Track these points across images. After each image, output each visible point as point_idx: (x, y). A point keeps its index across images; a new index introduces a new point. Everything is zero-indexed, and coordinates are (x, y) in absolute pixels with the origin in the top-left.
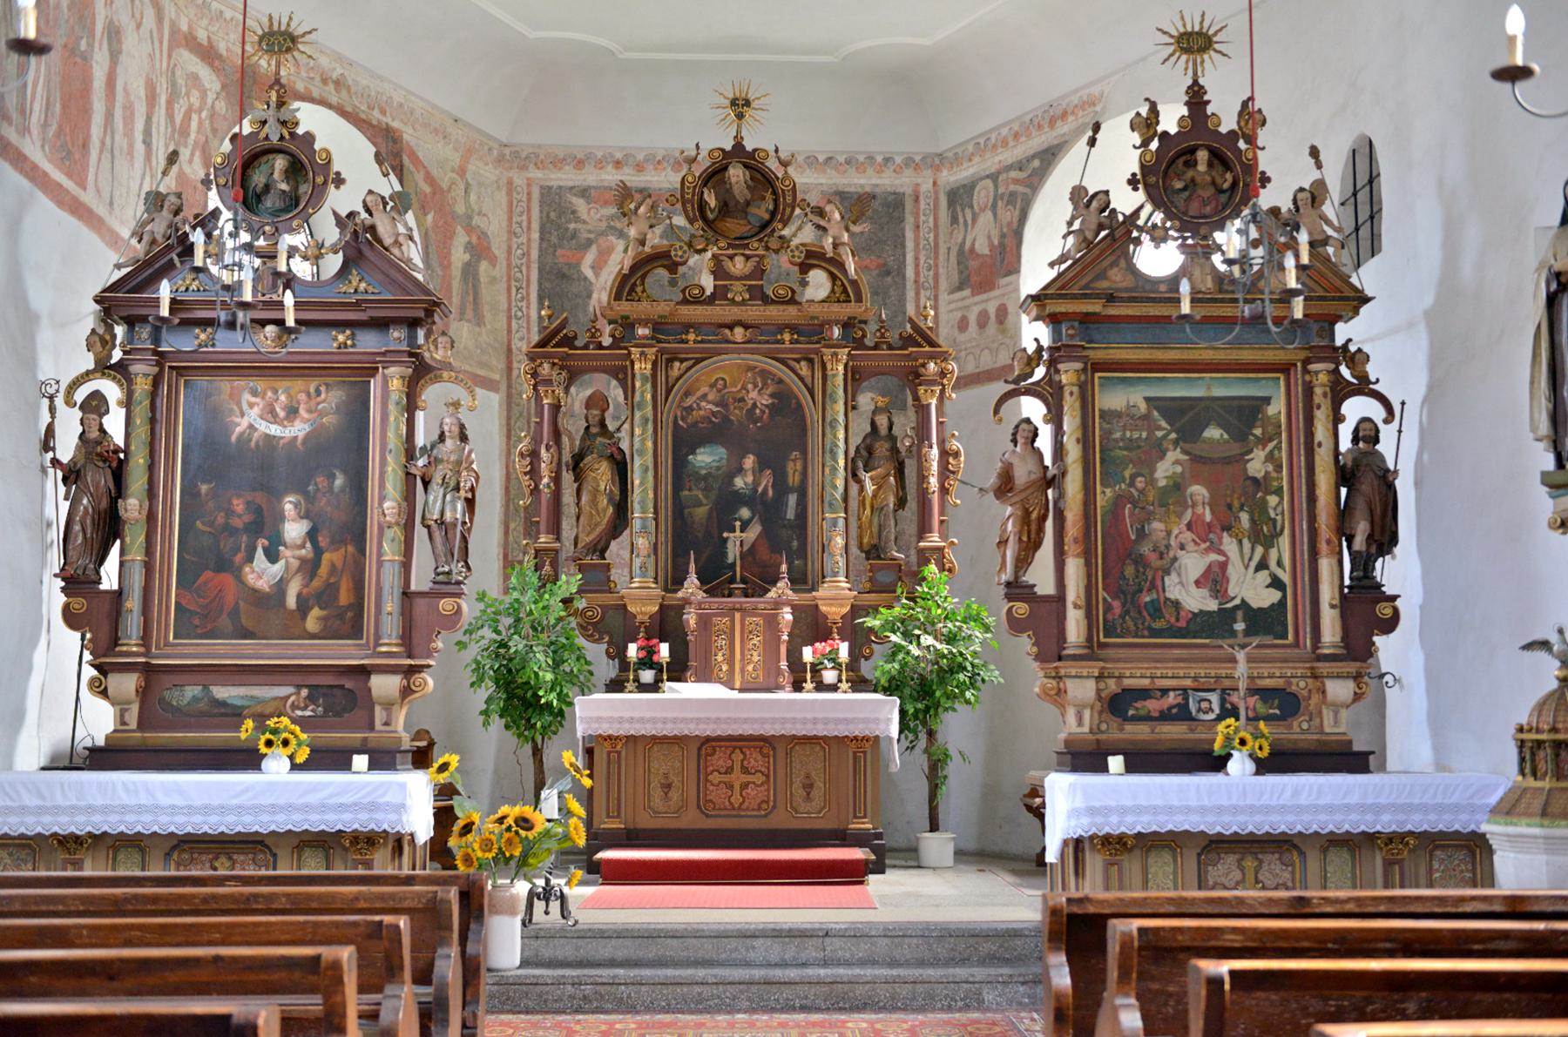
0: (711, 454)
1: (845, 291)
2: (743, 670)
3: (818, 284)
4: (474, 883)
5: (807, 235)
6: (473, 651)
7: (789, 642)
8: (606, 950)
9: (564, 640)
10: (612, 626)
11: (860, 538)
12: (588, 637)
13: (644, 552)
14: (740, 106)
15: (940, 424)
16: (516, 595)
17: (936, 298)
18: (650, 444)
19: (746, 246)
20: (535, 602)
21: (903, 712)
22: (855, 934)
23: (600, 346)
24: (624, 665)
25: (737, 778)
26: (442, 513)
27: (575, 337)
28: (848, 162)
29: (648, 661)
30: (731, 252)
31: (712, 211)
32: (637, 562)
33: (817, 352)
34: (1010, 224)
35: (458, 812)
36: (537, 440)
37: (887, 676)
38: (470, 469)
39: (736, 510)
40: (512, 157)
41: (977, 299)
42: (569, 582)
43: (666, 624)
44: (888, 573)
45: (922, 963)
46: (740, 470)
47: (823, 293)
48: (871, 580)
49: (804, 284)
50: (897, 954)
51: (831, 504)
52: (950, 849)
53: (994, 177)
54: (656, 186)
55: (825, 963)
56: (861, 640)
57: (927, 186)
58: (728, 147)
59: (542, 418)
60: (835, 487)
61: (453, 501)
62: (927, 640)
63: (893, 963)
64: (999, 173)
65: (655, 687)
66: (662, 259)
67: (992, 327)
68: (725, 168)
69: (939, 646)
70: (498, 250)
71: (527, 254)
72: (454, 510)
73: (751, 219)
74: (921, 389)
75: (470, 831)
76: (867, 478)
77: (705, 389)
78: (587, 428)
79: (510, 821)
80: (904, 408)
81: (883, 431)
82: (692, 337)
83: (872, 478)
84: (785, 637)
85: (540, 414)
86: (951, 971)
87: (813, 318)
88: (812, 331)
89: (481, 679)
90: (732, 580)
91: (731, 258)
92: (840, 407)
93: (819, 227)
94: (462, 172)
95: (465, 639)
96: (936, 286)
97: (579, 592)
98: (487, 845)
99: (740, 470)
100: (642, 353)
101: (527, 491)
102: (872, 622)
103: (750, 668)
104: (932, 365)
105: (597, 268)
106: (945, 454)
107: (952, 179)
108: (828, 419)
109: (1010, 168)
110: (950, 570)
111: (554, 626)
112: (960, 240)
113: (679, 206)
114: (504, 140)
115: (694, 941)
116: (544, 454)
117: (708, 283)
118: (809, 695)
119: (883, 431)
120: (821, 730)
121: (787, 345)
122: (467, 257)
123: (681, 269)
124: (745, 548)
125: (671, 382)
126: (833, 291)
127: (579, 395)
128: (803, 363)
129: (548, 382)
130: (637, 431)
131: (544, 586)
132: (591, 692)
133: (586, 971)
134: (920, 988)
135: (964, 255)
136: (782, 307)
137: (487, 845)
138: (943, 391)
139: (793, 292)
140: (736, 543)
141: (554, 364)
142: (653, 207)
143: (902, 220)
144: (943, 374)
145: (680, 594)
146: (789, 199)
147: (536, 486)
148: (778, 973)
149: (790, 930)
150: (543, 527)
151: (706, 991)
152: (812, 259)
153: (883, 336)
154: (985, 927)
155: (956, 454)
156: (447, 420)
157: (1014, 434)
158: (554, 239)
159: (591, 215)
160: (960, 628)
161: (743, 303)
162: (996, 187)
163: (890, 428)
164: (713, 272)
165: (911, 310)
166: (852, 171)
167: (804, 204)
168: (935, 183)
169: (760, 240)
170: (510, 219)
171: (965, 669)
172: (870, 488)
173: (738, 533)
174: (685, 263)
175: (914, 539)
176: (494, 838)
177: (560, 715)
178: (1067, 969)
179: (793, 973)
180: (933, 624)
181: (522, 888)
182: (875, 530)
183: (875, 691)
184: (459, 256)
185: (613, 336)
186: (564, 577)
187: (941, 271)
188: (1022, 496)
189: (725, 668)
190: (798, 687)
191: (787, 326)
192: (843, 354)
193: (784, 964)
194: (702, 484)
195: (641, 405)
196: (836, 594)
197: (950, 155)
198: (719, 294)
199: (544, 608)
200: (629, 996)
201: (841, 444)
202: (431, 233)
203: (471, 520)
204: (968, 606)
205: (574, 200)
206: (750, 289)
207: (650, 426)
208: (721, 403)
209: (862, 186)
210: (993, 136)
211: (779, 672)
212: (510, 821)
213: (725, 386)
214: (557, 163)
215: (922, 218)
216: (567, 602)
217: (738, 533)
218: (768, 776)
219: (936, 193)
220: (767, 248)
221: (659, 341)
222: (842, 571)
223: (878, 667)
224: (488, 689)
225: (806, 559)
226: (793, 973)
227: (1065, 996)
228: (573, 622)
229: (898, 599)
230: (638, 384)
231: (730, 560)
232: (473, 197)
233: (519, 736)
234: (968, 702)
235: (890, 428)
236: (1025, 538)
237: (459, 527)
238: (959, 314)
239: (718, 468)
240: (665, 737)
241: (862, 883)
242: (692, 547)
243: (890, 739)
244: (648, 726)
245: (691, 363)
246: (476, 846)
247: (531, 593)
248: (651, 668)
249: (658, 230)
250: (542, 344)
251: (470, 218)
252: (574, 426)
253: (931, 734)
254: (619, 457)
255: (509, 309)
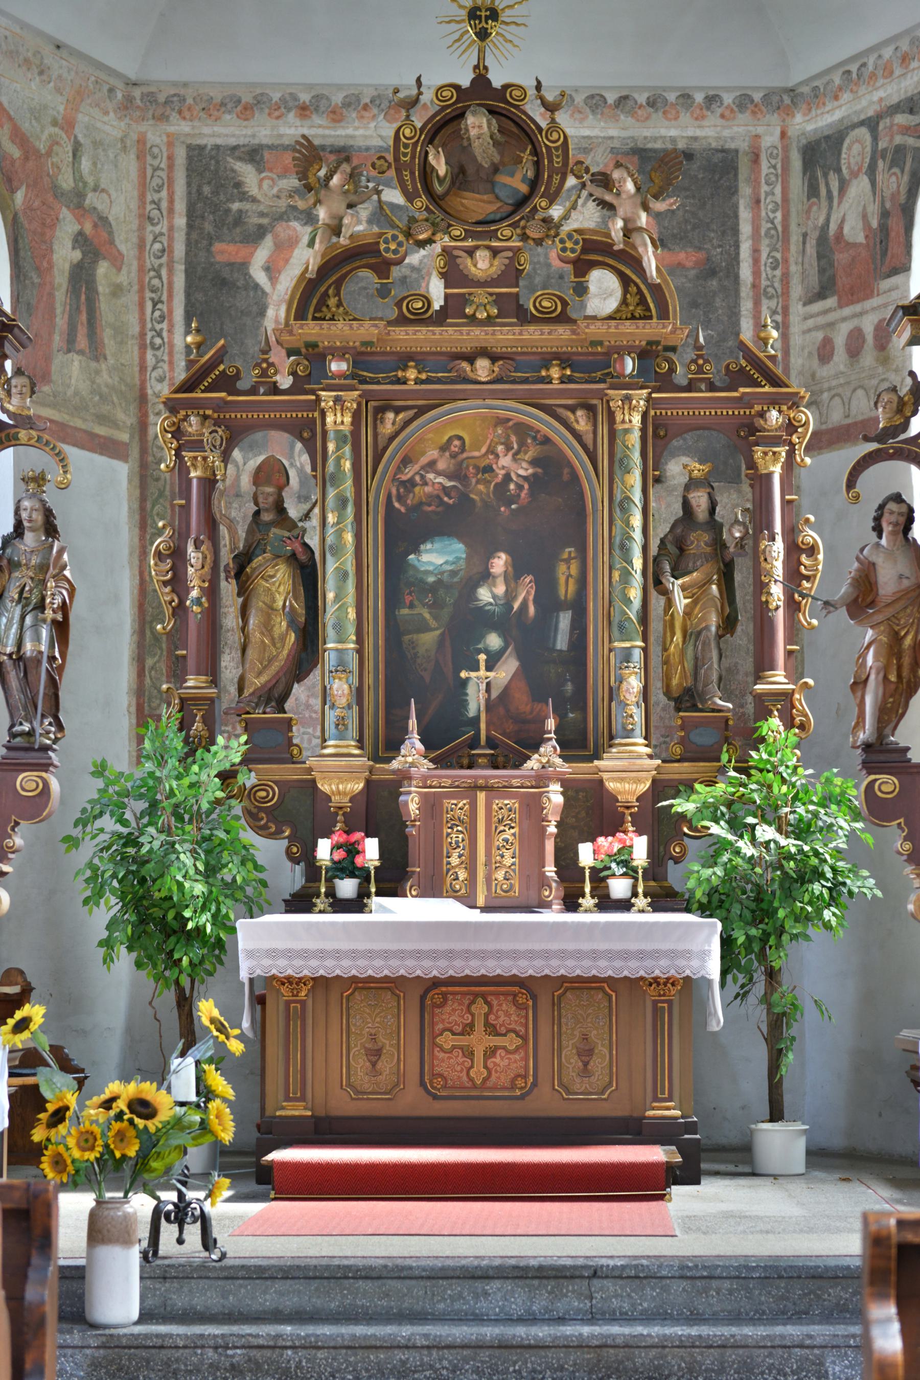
0: (440, 552)
1: (643, 301)
2: (488, 879)
3: (604, 290)
4: (36, 1196)
5: (586, 217)
6: (87, 851)
7: (557, 836)
8: (268, 1297)
9: (221, 834)
10: (297, 814)
11: (667, 678)
12: (261, 830)
13: (343, 702)
14: (483, 19)
15: (786, 504)
16: (149, 766)
17: (786, 311)
18: (349, 537)
19: (493, 235)
20: (179, 777)
21: (727, 942)
22: (636, 1274)
23: (275, 389)
24: (313, 871)
25: (480, 1041)
26: (20, 644)
27: (237, 376)
28: (652, 103)
29: (347, 866)
30: (469, 243)
31: (441, 181)
32: (331, 716)
33: (601, 395)
34: (893, 197)
35: (46, 1093)
36: (181, 535)
37: (705, 887)
38: (59, 577)
39: (482, 637)
40: (145, 101)
41: (847, 311)
42: (230, 749)
43: (377, 809)
44: (708, 728)
45: (736, 1318)
46: (486, 576)
47: (611, 305)
48: (682, 742)
49: (581, 290)
50: (701, 1304)
51: (621, 627)
52: (800, 1147)
53: (872, 124)
54: (361, 143)
55: (592, 1318)
56: (665, 830)
57: (770, 139)
58: (465, 82)
59: (188, 499)
60: (628, 601)
61: (35, 626)
62: (766, 832)
63: (695, 1318)
64: (879, 117)
65: (357, 905)
66: (364, 254)
67: (868, 357)
68: (461, 115)
69: (783, 841)
70: (125, 245)
71: (166, 251)
72: (37, 639)
73: (502, 194)
74: (759, 451)
75: (62, 1120)
76: (676, 586)
77: (433, 454)
78: (257, 514)
79: (121, 1104)
80: (734, 480)
81: (701, 512)
82: (412, 374)
83: (683, 588)
84: (552, 829)
85: (186, 492)
86: (779, 1330)
87: (594, 344)
88: (592, 365)
89: (99, 894)
90: (474, 743)
91: (471, 252)
92: (635, 478)
93: (604, 204)
94: (68, 125)
95: (77, 832)
96: (786, 293)
97: (245, 761)
98: (87, 1140)
99: (486, 576)
100: (337, 400)
101: (168, 611)
102: (684, 806)
103: (500, 875)
104: (774, 414)
105: (271, 270)
106: (794, 549)
107: (810, 127)
108: (618, 496)
109: (895, 109)
110: (802, 727)
111: (209, 813)
112: (821, 220)
113: (392, 173)
114: (132, 76)
115: (398, 1284)
116: (192, 554)
117: (437, 291)
118: (588, 916)
119: (701, 512)
120: (604, 969)
121: (556, 385)
122: (77, 255)
123: (396, 272)
124: (495, 694)
125: (381, 443)
126: (624, 302)
127: (244, 464)
128: (580, 413)
129: (197, 445)
130: (331, 518)
131: (192, 753)
132: (263, 913)
133: (235, 1329)
134: (732, 1356)
135: (827, 245)
136: (546, 328)
137: (87, 1140)
138: (791, 454)
139: (565, 303)
140: (485, 682)
141: (205, 417)
142: (353, 176)
143: (733, 191)
144: (791, 427)
145: (395, 764)
146: (557, 162)
147: (182, 602)
148: (521, 1331)
149: (541, 1268)
150: (191, 663)
151: (413, 1358)
152: (593, 252)
153: (700, 370)
154: (832, 1263)
155: (812, 551)
156: (26, 504)
157: (878, 519)
158: (208, 227)
159: (264, 188)
160: (816, 815)
161: (489, 321)
162: (875, 139)
163: (712, 511)
164: (443, 275)
165: (747, 334)
166: (657, 117)
167: (580, 169)
168: (783, 134)
169: (514, 225)
170: (142, 197)
171: (822, 875)
172: (681, 602)
173: (482, 672)
174: (400, 262)
175: (751, 679)
176: (97, 1130)
177: (220, 948)
178: (896, 1327)
179: (542, 1332)
180: (777, 808)
181: (141, 1205)
182: (689, 665)
183: (688, 910)
184: (65, 254)
185: (294, 373)
186: (220, 740)
187: (793, 268)
188: (889, 612)
189: (462, 875)
190: (571, 904)
191: (557, 356)
192: (640, 396)
193: (530, 1319)
194: (429, 599)
195: (336, 479)
196: (628, 769)
197: (806, 89)
198: (454, 309)
199: (192, 786)
200: (299, 1366)
201: (637, 535)
202: (22, 219)
203: (63, 655)
204: (828, 781)
205: (239, 166)
206: (499, 300)
207: (350, 510)
208: (458, 474)
209: (673, 140)
210: (871, 61)
211: (544, 882)
212: (121, 1104)
213: (463, 449)
214: (213, 107)
215: (764, 188)
216: (226, 777)
217: (482, 672)
218: (525, 1038)
219: (786, 149)
220: (524, 237)
221: (363, 381)
222: (639, 729)
223: (696, 876)
224: (109, 907)
225: (584, 709)
226: (542, 1332)
227: (893, 1365)
228: (237, 807)
229: (722, 770)
230: (331, 447)
231: (472, 712)
232: (85, 164)
233: (158, 978)
234: (827, 926)
235: (712, 511)
236: (893, 678)
237: (45, 664)
238: (820, 335)
239: (453, 573)
240: (370, 979)
241: (661, 1198)
242: (410, 695)
243: (709, 982)
244: (330, 963)
245: (411, 413)
246: (71, 1142)
247: (173, 762)
248: (352, 875)
249: (365, 211)
250: (188, 386)
251: (80, 195)
252: (237, 514)
253: (772, 975)
254: (303, 558)
255: (143, 335)
